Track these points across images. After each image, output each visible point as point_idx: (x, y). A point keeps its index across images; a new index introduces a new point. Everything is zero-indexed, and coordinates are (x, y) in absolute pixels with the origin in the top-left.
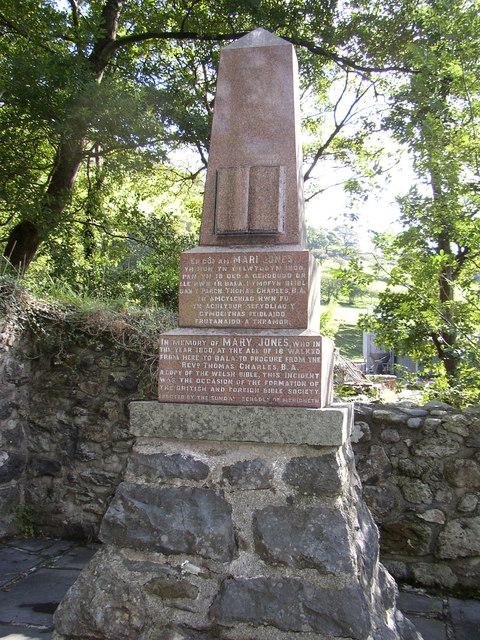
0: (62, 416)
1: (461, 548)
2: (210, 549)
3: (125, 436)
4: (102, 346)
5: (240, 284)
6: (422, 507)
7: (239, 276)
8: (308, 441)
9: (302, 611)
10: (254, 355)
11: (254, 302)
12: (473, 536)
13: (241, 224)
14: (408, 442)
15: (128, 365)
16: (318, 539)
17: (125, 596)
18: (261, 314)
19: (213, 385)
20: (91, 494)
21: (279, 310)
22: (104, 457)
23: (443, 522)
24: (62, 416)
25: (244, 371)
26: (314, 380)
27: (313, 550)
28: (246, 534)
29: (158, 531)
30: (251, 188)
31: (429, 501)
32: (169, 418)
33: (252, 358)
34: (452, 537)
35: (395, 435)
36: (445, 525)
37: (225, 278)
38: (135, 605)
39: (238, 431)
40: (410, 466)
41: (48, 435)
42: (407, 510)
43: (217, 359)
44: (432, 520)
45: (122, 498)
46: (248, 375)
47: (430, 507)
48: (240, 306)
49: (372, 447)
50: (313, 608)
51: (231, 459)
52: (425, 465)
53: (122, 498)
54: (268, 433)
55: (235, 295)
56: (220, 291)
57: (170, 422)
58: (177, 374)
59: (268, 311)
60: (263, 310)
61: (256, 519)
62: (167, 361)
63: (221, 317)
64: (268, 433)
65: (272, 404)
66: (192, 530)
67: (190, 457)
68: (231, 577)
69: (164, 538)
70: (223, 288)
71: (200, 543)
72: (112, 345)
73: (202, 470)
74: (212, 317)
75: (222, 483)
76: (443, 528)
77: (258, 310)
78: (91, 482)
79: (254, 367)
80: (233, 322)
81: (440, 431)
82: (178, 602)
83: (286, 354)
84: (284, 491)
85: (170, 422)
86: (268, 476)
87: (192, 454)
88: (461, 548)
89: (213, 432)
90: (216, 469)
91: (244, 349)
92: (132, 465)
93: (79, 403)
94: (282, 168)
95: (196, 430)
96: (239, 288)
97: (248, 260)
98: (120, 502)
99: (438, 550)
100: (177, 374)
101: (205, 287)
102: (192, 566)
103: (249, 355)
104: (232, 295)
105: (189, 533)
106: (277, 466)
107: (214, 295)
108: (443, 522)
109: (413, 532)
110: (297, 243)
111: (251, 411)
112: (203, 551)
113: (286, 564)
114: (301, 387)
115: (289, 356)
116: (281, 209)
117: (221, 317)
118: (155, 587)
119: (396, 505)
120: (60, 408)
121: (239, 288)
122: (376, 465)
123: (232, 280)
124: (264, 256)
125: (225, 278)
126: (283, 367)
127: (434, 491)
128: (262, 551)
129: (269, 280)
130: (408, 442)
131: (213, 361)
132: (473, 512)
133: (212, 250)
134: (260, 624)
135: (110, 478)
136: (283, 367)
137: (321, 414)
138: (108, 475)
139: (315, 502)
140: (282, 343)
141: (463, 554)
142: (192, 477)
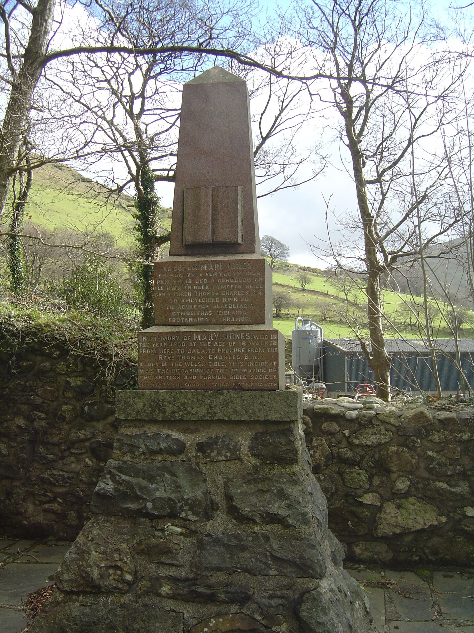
0: (21, 422)
1: (396, 526)
2: (190, 513)
3: (82, 437)
4: (58, 353)
5: (207, 287)
6: (360, 491)
7: (206, 281)
8: (270, 418)
9: (270, 559)
10: (221, 348)
11: (220, 303)
12: (406, 515)
13: (206, 237)
14: (347, 433)
15: (84, 371)
16: (280, 499)
17: (116, 556)
18: (226, 313)
19: (186, 374)
20: (50, 494)
21: (242, 309)
22: (63, 458)
23: (379, 504)
24: (21, 422)
25: (213, 361)
26: (272, 367)
27: (278, 508)
28: (218, 498)
29: (144, 499)
30: (213, 206)
31: (367, 486)
32: (149, 402)
33: (219, 350)
34: (388, 517)
35: (335, 427)
36: (382, 506)
37: (193, 283)
38: (126, 563)
39: (210, 411)
40: (349, 455)
41: (6, 440)
42: (347, 495)
43: (189, 352)
44: (369, 503)
45: (110, 473)
46: (216, 364)
47: (367, 492)
48: (207, 306)
49: (314, 439)
50: (278, 555)
51: (202, 437)
52: (362, 453)
53: (110, 473)
54: (236, 412)
55: (203, 297)
56: (190, 294)
57: (150, 406)
58: (155, 366)
59: (231, 310)
60: (227, 309)
61: (253, 455)
62: (146, 354)
63: (191, 316)
64: (236, 412)
65: (238, 388)
66: (173, 496)
67: (168, 436)
68: (209, 535)
69: (149, 505)
70: (192, 291)
71: (181, 507)
72: (68, 351)
73: (181, 448)
74: (183, 316)
75: (196, 457)
76: (380, 509)
77: (224, 310)
78: (51, 483)
79: (221, 358)
80: (202, 320)
81: (374, 421)
82: (164, 559)
83: (248, 345)
84: (251, 461)
85: (150, 406)
86: (236, 448)
87: (170, 433)
88: (396, 526)
89: (189, 413)
90: (191, 445)
91: (213, 342)
92: (118, 444)
93: (36, 407)
94: (240, 189)
95: (174, 412)
96: (206, 291)
97: (214, 268)
98: (108, 476)
99: (376, 529)
100: (155, 366)
101: (176, 291)
102: (174, 528)
103: (216, 348)
104: (201, 297)
105: (170, 499)
106: (244, 441)
107: (185, 298)
108: (379, 504)
109: (353, 514)
110: (254, 252)
111: (221, 394)
112: (183, 514)
113: (255, 522)
114: (262, 374)
115: (251, 347)
116: (240, 223)
117: (191, 316)
118: (143, 547)
119: (337, 490)
120: (17, 413)
121: (206, 291)
122: (317, 454)
123: (200, 284)
124: (229, 262)
125: (193, 283)
126: (246, 357)
127: (370, 477)
128: (233, 511)
129: (232, 283)
130: (347, 433)
131: (186, 354)
132: (406, 493)
133: (182, 259)
134: (235, 571)
135: (69, 478)
136: (246, 357)
137: (280, 395)
138: (66, 475)
139: (278, 470)
140: (245, 337)
141: (398, 531)
142: (170, 452)
